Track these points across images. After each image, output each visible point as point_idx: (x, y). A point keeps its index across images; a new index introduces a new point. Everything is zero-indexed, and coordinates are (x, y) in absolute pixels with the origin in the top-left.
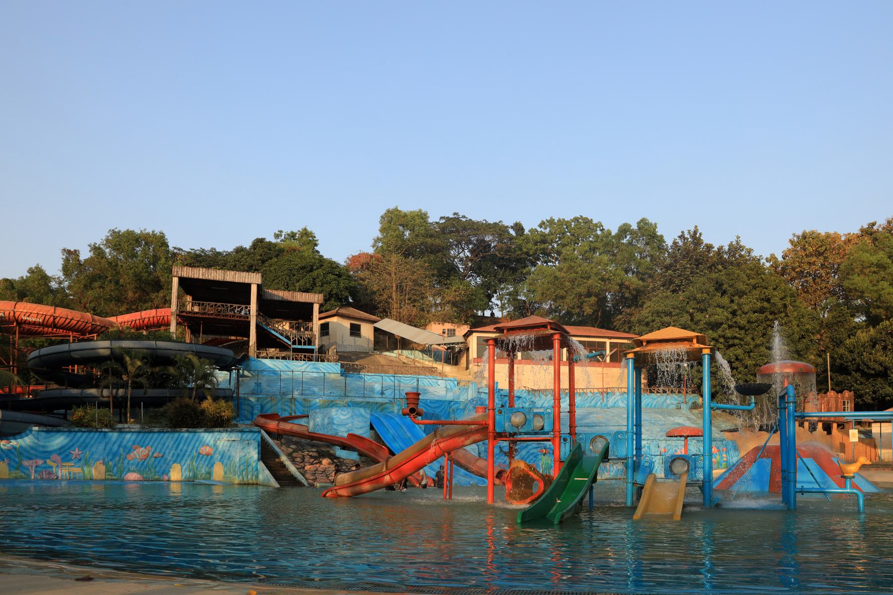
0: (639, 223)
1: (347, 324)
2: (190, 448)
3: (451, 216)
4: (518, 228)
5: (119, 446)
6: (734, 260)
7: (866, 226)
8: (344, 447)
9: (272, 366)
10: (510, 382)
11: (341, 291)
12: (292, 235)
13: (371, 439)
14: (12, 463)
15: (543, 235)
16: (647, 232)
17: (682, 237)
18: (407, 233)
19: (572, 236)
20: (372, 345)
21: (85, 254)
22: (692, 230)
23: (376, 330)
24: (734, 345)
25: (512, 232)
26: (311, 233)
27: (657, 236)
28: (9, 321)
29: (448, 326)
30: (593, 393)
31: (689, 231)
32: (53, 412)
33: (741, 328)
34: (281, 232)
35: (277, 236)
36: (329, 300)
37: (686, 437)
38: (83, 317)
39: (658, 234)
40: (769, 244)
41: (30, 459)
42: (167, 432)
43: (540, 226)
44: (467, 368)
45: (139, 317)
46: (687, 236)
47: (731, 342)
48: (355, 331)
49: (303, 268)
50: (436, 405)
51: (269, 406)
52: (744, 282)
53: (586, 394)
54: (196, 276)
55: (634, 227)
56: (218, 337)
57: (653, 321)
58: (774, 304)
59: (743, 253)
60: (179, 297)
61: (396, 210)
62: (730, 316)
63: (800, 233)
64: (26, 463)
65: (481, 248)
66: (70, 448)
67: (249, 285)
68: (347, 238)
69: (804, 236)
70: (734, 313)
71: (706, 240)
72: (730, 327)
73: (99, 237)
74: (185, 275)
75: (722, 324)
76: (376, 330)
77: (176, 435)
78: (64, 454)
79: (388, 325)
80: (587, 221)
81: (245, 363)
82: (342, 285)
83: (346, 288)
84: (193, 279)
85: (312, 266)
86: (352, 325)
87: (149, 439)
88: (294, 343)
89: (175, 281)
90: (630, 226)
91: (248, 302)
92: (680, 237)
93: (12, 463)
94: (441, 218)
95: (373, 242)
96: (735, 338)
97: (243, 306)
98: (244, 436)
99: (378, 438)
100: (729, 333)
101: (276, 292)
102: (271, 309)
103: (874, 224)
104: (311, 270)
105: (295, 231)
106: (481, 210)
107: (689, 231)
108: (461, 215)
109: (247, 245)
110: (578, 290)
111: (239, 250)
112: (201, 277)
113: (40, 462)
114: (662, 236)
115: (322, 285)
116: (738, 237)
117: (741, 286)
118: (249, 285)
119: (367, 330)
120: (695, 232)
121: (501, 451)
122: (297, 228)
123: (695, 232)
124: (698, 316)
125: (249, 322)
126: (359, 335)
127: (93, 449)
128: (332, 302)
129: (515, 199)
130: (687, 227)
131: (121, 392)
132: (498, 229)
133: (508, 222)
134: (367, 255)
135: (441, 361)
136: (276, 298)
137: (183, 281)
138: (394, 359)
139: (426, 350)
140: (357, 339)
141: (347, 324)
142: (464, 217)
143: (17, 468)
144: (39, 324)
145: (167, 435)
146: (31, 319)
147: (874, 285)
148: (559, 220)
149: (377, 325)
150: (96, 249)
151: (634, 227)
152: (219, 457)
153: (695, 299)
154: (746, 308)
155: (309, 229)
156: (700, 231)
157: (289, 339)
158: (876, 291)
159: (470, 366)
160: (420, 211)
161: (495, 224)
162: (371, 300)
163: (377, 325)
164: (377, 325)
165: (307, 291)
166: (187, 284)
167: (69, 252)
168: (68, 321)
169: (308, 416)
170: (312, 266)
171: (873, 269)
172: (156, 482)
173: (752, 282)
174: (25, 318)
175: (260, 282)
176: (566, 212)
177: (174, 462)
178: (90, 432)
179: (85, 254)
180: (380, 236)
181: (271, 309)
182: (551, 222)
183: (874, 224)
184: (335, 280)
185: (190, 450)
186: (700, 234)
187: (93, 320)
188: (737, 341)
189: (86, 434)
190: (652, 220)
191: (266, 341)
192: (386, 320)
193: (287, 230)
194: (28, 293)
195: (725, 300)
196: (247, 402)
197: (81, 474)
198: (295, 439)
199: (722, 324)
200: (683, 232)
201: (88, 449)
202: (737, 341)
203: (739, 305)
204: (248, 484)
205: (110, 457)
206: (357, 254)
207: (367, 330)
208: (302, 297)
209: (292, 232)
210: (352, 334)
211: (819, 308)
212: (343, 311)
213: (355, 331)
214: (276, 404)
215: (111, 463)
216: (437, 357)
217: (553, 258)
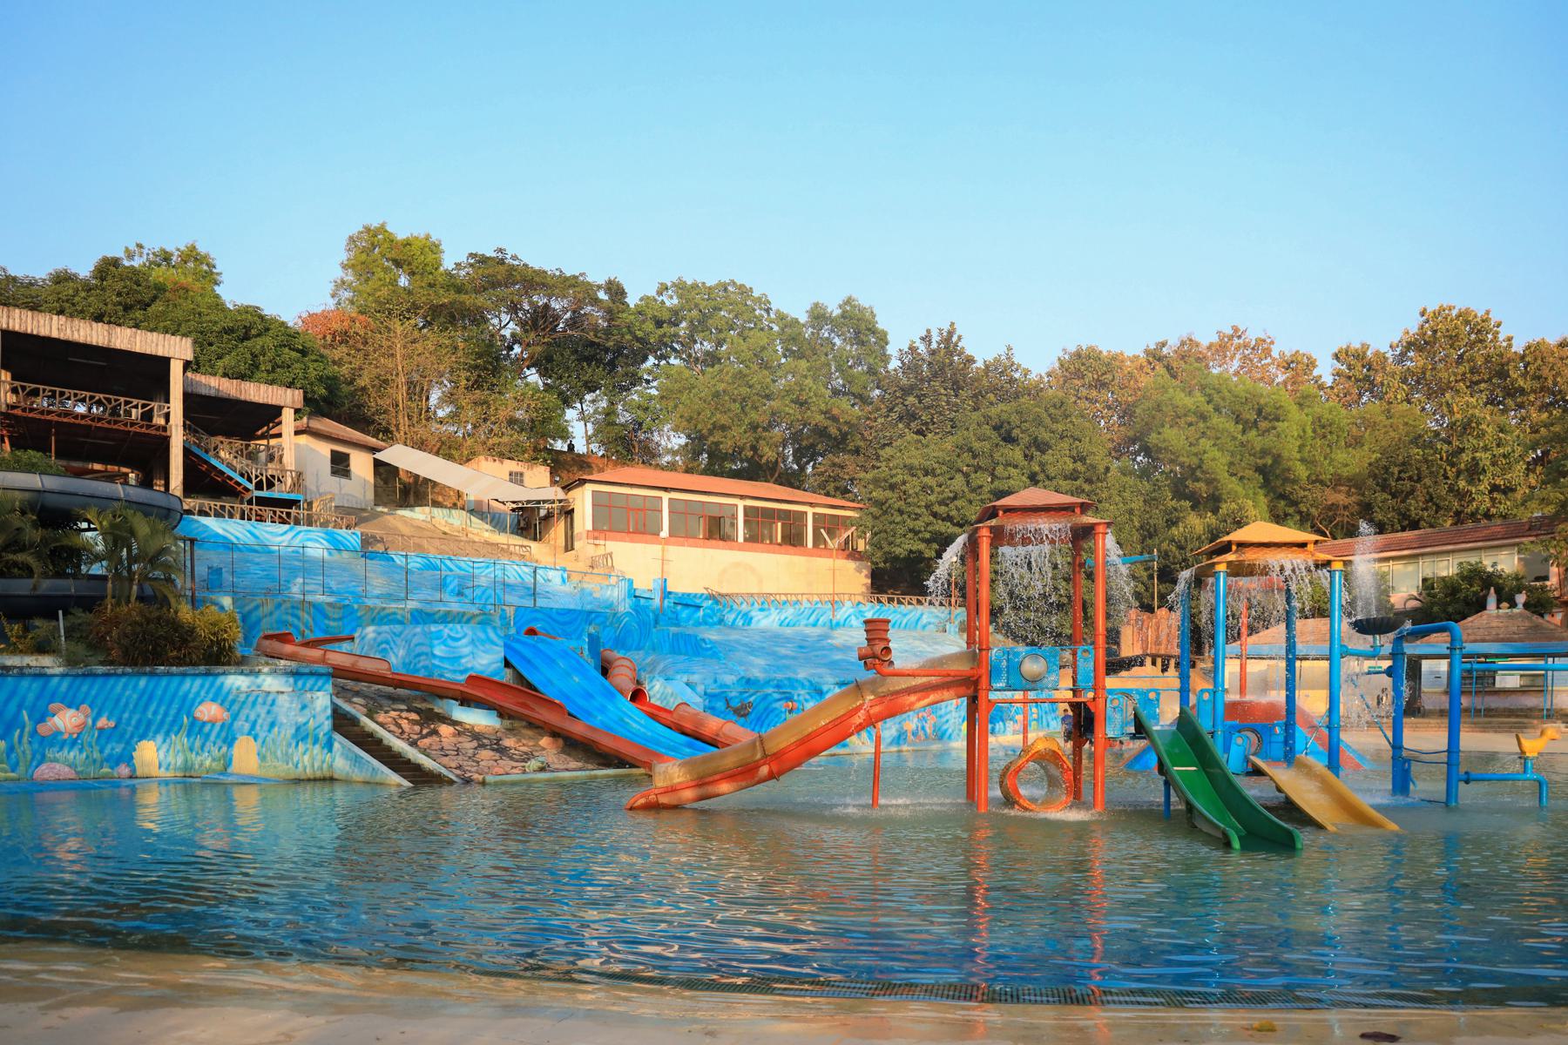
1: (324, 450)
2: (175, 706)
3: (490, 253)
5: (20, 707)
6: (1001, 382)
7: (1152, 347)
8: (466, 701)
9: (220, 531)
10: (1288, 639)
11: (311, 384)
13: (511, 683)
16: (859, 326)
17: (926, 339)
18: (403, 281)
19: (709, 313)
20: (370, 495)
22: (946, 327)
23: (378, 464)
25: (602, 295)
26: (206, 257)
29: (512, 466)
39: (880, 326)
40: (1038, 361)
42: (124, 674)
44: (569, 547)
46: (935, 338)
48: (340, 464)
50: (566, 618)
54: (44, 332)
57: (904, 483)
58: (1093, 467)
59: (1017, 375)
61: (382, 229)
63: (1072, 349)
65: (540, 320)
67: (165, 362)
68: (288, 276)
69: (1078, 355)
76: (378, 464)
77: (143, 682)
79: (402, 457)
80: (744, 291)
83: (320, 379)
85: (247, 329)
87: (85, 688)
88: (259, 486)
92: (923, 339)
94: (471, 255)
95: (332, 286)
98: (300, 683)
99: (520, 677)
102: (209, 415)
103: (1164, 344)
104: (246, 337)
105: (170, 248)
106: (539, 252)
108: (510, 252)
109: (84, 269)
110: (754, 415)
111: (62, 278)
112: (55, 334)
116: (1009, 348)
118: (165, 362)
119: (361, 464)
120: (951, 333)
121: (728, 706)
122: (175, 244)
123: (951, 333)
129: (615, 237)
130: (937, 324)
133: (597, 277)
134: (325, 315)
135: (504, 531)
136: (204, 391)
138: (424, 525)
139: (478, 511)
140: (344, 481)
141: (324, 450)
142: (514, 257)
145: (124, 680)
147: (1191, 445)
152: (247, 726)
153: (970, 450)
155: (202, 249)
157: (250, 480)
158: (1196, 454)
159: (577, 545)
160: (428, 237)
161: (575, 277)
162: (359, 406)
163: (379, 456)
164: (379, 456)
165: (242, 377)
169: (352, 639)
170: (247, 329)
171: (1189, 419)
173: (1060, 427)
175: (190, 357)
177: (143, 737)
180: (632, 300)
181: (202, 411)
182: (680, 287)
183: (1164, 344)
185: (172, 712)
186: (960, 338)
191: (203, 481)
195: (1016, 454)
198: (363, 686)
200: (928, 331)
203: (1042, 465)
204: (315, 780)
207: (361, 464)
208: (256, 392)
210: (334, 472)
211: (1493, 511)
213: (340, 464)
216: (496, 522)
217: (674, 350)
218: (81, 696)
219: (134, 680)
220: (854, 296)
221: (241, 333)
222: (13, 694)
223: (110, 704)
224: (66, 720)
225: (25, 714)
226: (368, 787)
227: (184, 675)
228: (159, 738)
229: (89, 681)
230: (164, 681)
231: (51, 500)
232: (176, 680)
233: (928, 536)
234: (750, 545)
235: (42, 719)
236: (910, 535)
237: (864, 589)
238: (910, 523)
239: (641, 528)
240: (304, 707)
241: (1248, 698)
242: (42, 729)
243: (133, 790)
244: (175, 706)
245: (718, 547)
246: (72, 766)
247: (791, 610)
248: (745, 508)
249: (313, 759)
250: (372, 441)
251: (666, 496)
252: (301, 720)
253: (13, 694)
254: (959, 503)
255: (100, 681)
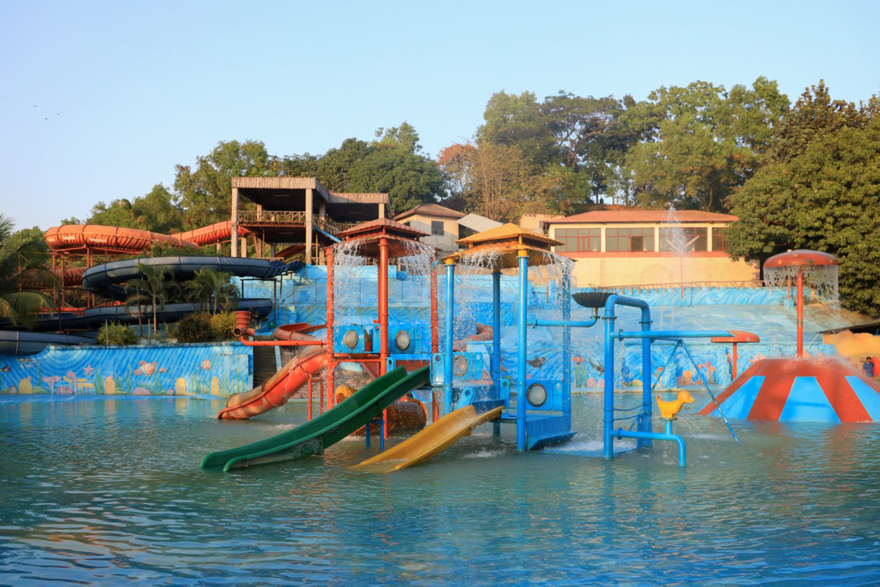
0: (755, 84)
2: (194, 361)
3: (558, 95)
4: (629, 101)
5: (127, 362)
12: (394, 131)
14: (35, 380)
15: (651, 107)
16: (767, 92)
21: (194, 169)
22: (817, 85)
24: (844, 226)
27: (780, 97)
28: (80, 244)
30: (675, 289)
31: (813, 86)
32: (81, 329)
33: (855, 204)
34: (382, 129)
35: (379, 134)
36: (409, 197)
37: (735, 343)
38: (142, 235)
39: (781, 93)
41: (50, 376)
43: (650, 97)
45: (225, 227)
46: (812, 94)
47: (842, 221)
49: (383, 166)
51: (305, 315)
52: (864, 146)
53: (666, 290)
54: (253, 186)
55: (750, 88)
56: (294, 244)
60: (240, 208)
62: (844, 189)
64: (46, 380)
65: (593, 126)
66: (83, 365)
67: (304, 191)
70: (849, 185)
71: (834, 96)
72: (838, 204)
73: (207, 149)
74: (243, 186)
75: (828, 200)
76: (462, 228)
78: (78, 368)
80: (706, 86)
81: (302, 270)
82: (422, 181)
83: (428, 184)
84: (259, 189)
85: (392, 164)
86: (433, 223)
87: (154, 354)
89: (235, 192)
90: (744, 87)
91: (303, 208)
93: (35, 380)
96: (848, 216)
97: (299, 213)
98: (236, 350)
100: (838, 211)
101: (341, 195)
107: (813, 86)
112: (258, 187)
113: (58, 378)
114: (785, 96)
115: (401, 184)
117: (858, 151)
118: (304, 191)
119: (450, 228)
122: (398, 125)
123: (821, 87)
124: (803, 192)
125: (305, 228)
126: (442, 233)
127: (104, 366)
128: (413, 199)
131: (149, 309)
132: (607, 104)
133: (619, 96)
136: (341, 201)
137: (241, 191)
140: (439, 237)
142: (571, 94)
143: (39, 385)
144: (104, 245)
146: (98, 241)
148: (672, 89)
149: (462, 222)
150: (203, 162)
151: (750, 88)
154: (863, 178)
155: (409, 123)
156: (826, 86)
163: (461, 222)
166: (247, 194)
167: (182, 169)
168: (129, 240)
170: (392, 164)
172: (164, 398)
174: (92, 240)
175: (314, 187)
176: (682, 79)
177: (179, 376)
178: (100, 349)
179: (194, 169)
182: (662, 91)
184: (415, 176)
185: (192, 365)
186: (827, 89)
187: (153, 237)
188: (849, 221)
189: (96, 352)
190: (770, 79)
192: (472, 216)
193: (388, 126)
194: (143, 211)
196: (284, 312)
197: (94, 390)
199: (828, 200)
201: (99, 366)
202: (849, 221)
205: (119, 373)
206: (450, 145)
207: (450, 228)
208: (366, 198)
209: (394, 129)
212: (424, 209)
214: (312, 313)
215: (120, 379)
218: (152, 358)
219: (175, 350)
220: (764, 75)
221: (389, 167)
222: (125, 356)
223: (165, 361)
224: (146, 368)
225: (129, 366)
226: (195, 402)
227: (197, 347)
228: (186, 377)
229: (156, 351)
230: (189, 349)
231: (184, 268)
232: (194, 349)
233: (763, 237)
234: (714, 253)
235: (135, 369)
236: (750, 238)
237: (754, 277)
238: (748, 229)
239: (586, 248)
240: (234, 362)
241: (805, 356)
242: (136, 372)
243: (174, 400)
244: (194, 361)
245: (615, 256)
246: (148, 389)
247: (657, 295)
248: (713, 229)
249: (238, 388)
250: (457, 213)
251: (603, 228)
252: (233, 368)
253: (125, 356)
254: (788, 211)
255: (161, 350)
